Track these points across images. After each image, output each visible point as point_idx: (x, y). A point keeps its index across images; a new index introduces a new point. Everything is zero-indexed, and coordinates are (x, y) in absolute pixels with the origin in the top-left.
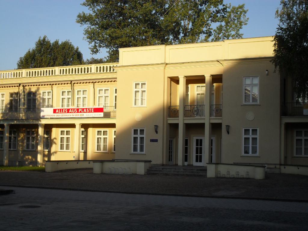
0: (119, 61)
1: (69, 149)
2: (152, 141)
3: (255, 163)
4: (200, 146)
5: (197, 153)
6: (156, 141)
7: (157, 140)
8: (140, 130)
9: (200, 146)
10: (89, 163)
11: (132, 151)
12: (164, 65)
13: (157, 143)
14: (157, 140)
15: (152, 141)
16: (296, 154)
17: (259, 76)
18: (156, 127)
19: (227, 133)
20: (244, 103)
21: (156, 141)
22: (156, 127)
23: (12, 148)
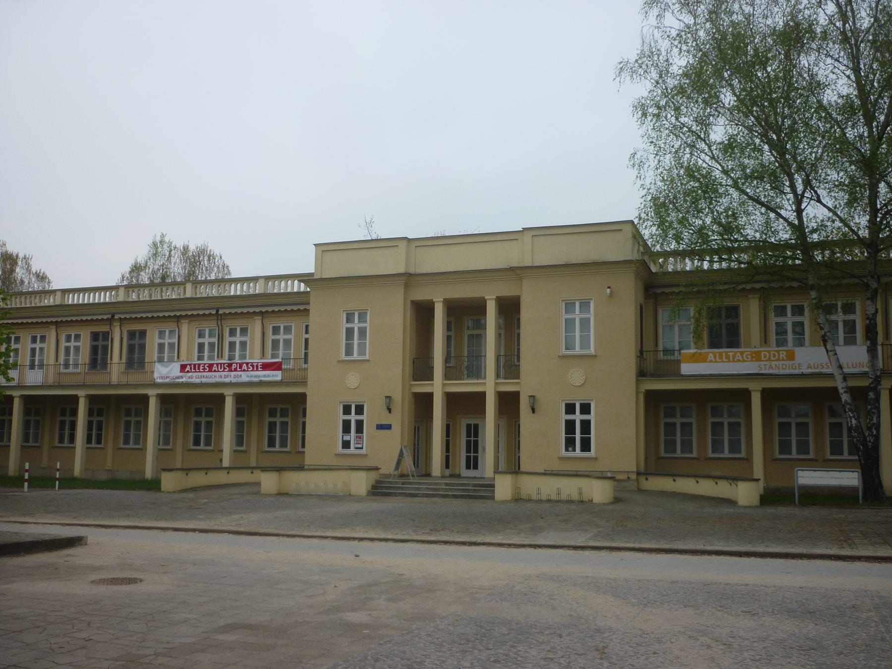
2: (380, 427)
6: (388, 427)
7: (377, 429)
15: (380, 427)
21: (388, 427)
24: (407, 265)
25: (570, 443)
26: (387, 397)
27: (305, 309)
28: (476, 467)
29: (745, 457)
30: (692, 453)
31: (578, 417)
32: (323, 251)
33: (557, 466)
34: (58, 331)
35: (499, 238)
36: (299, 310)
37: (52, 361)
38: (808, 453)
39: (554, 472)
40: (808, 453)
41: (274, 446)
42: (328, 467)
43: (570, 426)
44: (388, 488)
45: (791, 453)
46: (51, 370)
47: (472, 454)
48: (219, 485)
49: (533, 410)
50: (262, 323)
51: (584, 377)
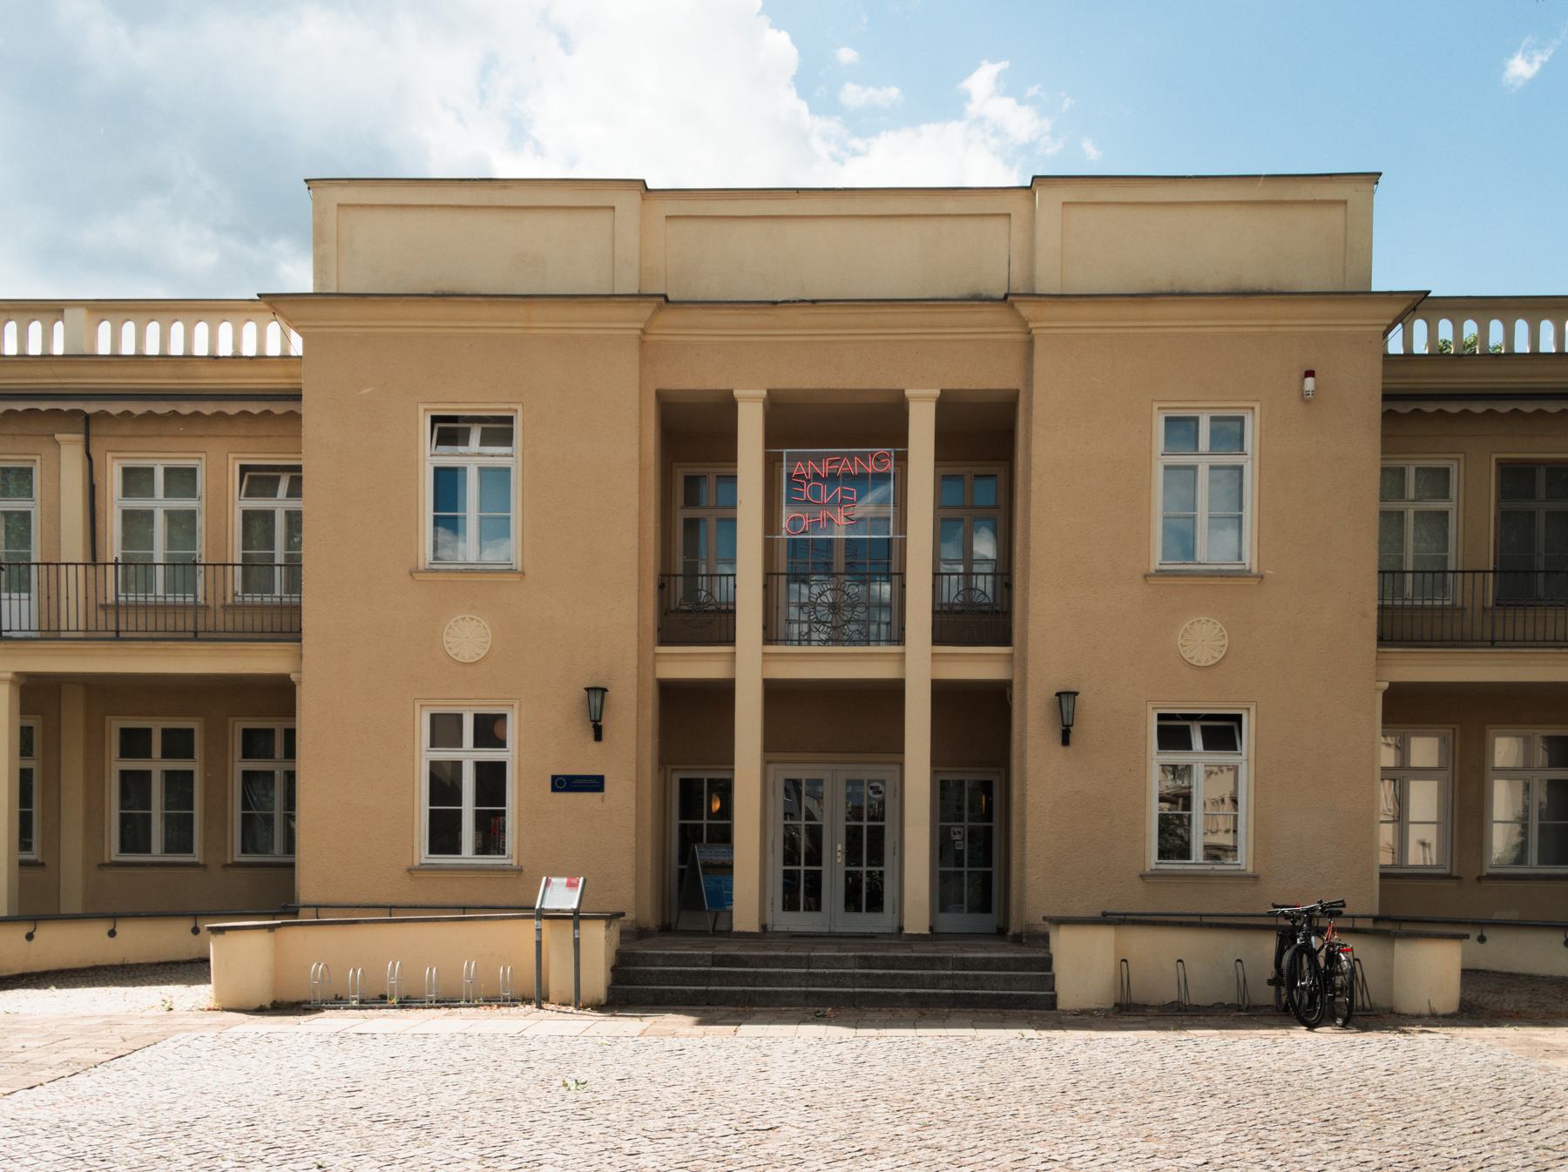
0: (304, 490)
1: (501, 850)
2: (563, 784)
3: (1148, 911)
4: (860, 828)
5: (852, 855)
6: (594, 784)
7: (554, 789)
8: (478, 718)
9: (860, 828)
10: (112, 934)
11: (421, 852)
12: (646, 310)
13: (598, 795)
14: (554, 789)
15: (563, 784)
16: (244, 851)
17: (1257, 406)
18: (597, 693)
19: (1060, 740)
20: (239, 857)
21: (594, 784)
22: (597, 693)
23: (966, 864)
24: (338, 288)
25: (444, 836)
26: (596, 689)
27: (292, 412)
28: (876, 903)
29: (201, 862)
30: (191, 851)
31: (468, 755)
32: (1064, 203)
33: (1136, 899)
34: (94, 442)
35: (950, 206)
36: (150, 415)
37: (73, 547)
38: (190, 850)
39: (1205, 920)
40: (190, 850)
41: (455, 848)
42: (1197, 919)
43: (444, 785)
44: (767, 979)
45: (147, 850)
46: (73, 583)
47: (864, 869)
48: (33, 974)
49: (1066, 740)
50: (88, 454)
51: (1226, 642)
